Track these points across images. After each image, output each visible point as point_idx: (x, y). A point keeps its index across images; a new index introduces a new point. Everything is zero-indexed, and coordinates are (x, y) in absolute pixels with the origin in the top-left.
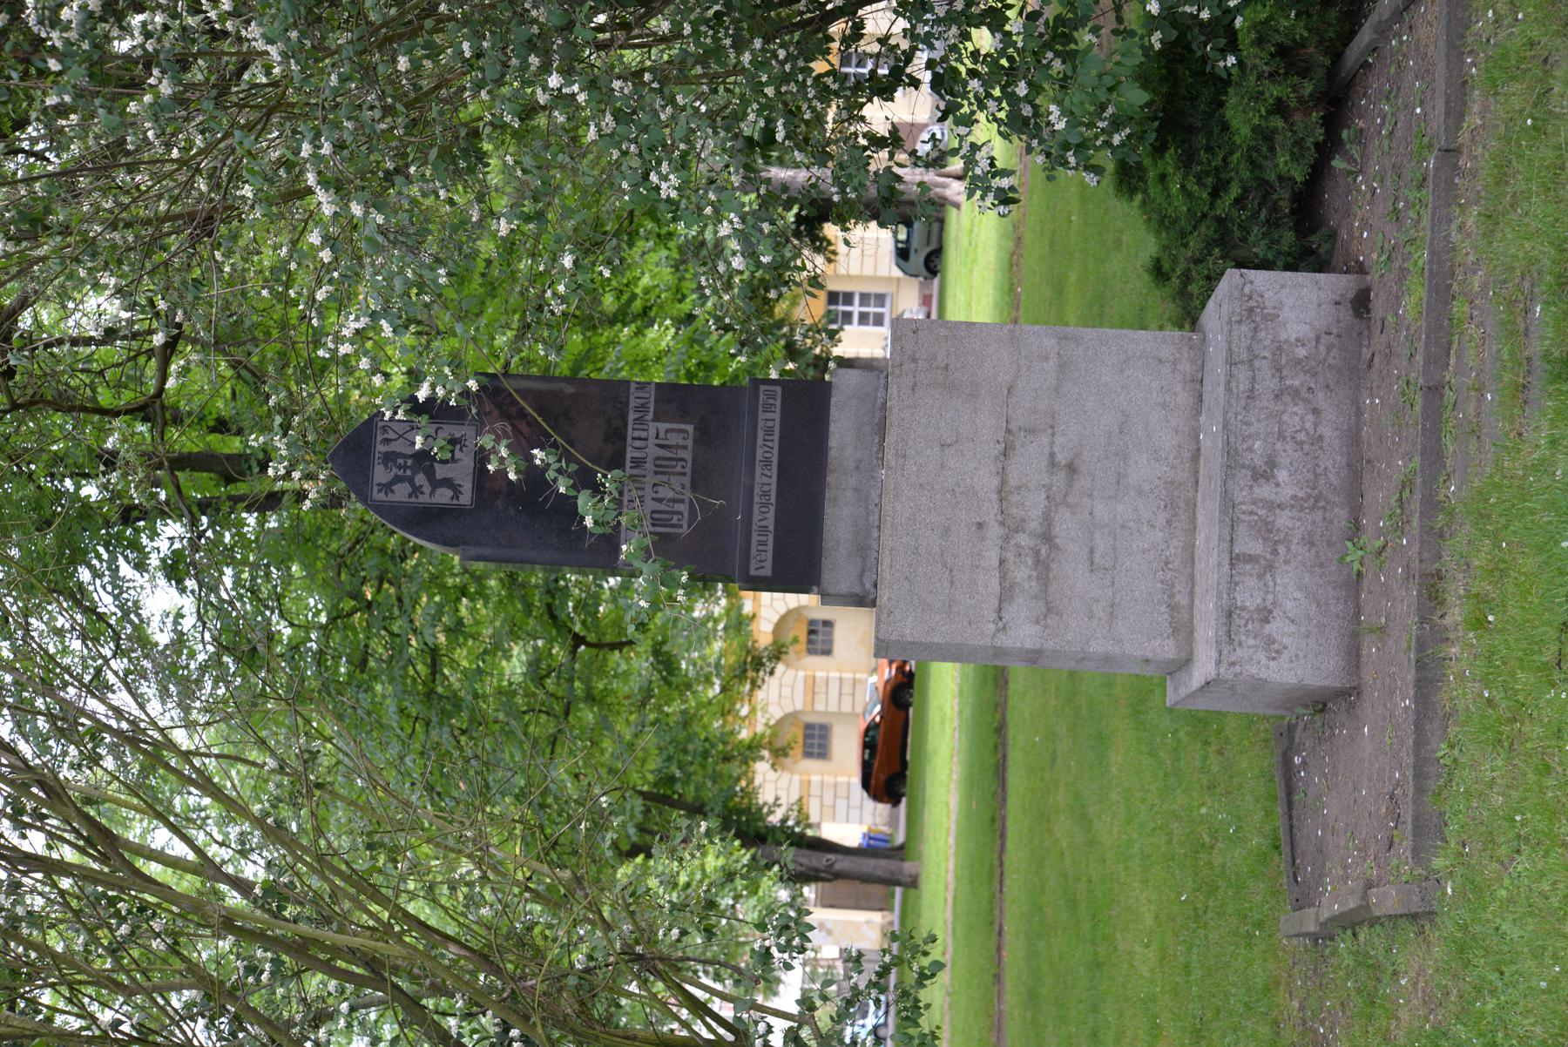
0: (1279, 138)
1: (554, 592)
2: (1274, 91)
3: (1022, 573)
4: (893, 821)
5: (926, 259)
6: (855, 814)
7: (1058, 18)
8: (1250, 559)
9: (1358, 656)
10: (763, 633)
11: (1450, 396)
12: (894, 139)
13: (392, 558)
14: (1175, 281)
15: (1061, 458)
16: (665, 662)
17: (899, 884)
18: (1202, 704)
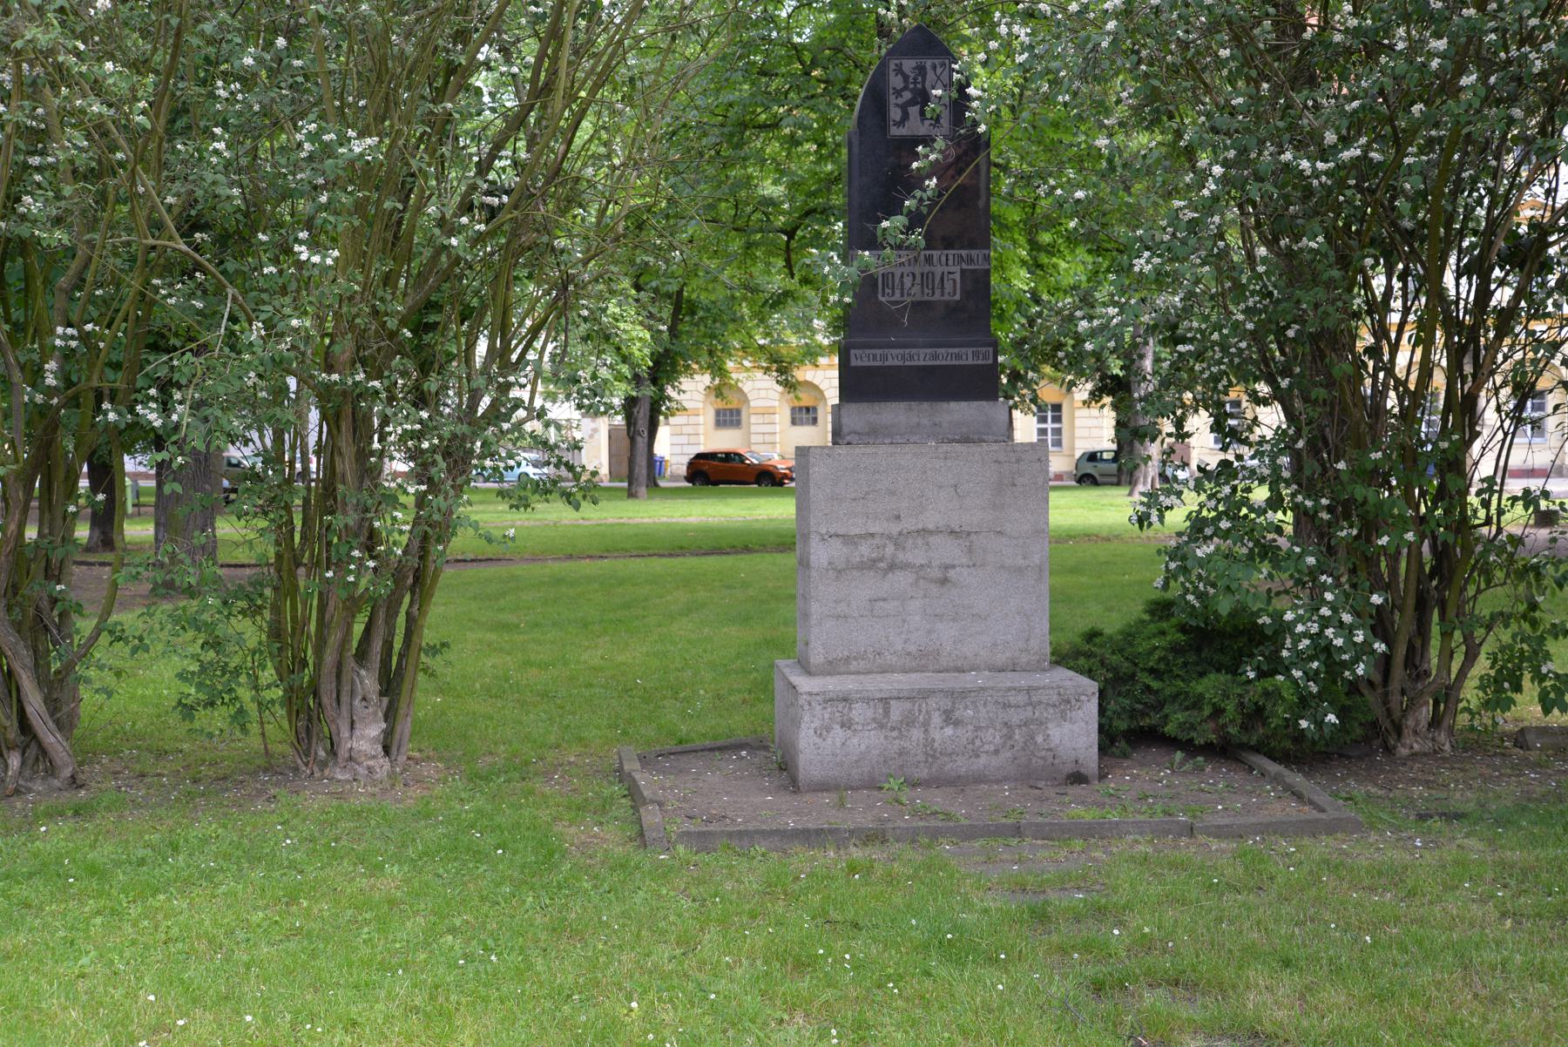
0: (1195, 713)
1: (825, 213)
2: (1230, 707)
3: (865, 550)
4: (674, 478)
5: (1090, 473)
6: (678, 450)
7: (1279, 548)
8: (887, 712)
9: (822, 791)
10: (805, 374)
11: (1014, 842)
12: (1182, 435)
13: (844, 89)
14: (1087, 647)
15: (952, 574)
16: (779, 301)
17: (630, 484)
18: (778, 685)
